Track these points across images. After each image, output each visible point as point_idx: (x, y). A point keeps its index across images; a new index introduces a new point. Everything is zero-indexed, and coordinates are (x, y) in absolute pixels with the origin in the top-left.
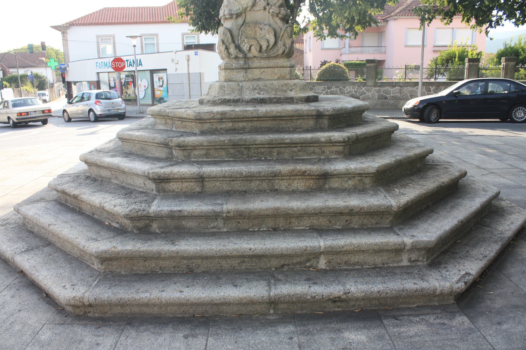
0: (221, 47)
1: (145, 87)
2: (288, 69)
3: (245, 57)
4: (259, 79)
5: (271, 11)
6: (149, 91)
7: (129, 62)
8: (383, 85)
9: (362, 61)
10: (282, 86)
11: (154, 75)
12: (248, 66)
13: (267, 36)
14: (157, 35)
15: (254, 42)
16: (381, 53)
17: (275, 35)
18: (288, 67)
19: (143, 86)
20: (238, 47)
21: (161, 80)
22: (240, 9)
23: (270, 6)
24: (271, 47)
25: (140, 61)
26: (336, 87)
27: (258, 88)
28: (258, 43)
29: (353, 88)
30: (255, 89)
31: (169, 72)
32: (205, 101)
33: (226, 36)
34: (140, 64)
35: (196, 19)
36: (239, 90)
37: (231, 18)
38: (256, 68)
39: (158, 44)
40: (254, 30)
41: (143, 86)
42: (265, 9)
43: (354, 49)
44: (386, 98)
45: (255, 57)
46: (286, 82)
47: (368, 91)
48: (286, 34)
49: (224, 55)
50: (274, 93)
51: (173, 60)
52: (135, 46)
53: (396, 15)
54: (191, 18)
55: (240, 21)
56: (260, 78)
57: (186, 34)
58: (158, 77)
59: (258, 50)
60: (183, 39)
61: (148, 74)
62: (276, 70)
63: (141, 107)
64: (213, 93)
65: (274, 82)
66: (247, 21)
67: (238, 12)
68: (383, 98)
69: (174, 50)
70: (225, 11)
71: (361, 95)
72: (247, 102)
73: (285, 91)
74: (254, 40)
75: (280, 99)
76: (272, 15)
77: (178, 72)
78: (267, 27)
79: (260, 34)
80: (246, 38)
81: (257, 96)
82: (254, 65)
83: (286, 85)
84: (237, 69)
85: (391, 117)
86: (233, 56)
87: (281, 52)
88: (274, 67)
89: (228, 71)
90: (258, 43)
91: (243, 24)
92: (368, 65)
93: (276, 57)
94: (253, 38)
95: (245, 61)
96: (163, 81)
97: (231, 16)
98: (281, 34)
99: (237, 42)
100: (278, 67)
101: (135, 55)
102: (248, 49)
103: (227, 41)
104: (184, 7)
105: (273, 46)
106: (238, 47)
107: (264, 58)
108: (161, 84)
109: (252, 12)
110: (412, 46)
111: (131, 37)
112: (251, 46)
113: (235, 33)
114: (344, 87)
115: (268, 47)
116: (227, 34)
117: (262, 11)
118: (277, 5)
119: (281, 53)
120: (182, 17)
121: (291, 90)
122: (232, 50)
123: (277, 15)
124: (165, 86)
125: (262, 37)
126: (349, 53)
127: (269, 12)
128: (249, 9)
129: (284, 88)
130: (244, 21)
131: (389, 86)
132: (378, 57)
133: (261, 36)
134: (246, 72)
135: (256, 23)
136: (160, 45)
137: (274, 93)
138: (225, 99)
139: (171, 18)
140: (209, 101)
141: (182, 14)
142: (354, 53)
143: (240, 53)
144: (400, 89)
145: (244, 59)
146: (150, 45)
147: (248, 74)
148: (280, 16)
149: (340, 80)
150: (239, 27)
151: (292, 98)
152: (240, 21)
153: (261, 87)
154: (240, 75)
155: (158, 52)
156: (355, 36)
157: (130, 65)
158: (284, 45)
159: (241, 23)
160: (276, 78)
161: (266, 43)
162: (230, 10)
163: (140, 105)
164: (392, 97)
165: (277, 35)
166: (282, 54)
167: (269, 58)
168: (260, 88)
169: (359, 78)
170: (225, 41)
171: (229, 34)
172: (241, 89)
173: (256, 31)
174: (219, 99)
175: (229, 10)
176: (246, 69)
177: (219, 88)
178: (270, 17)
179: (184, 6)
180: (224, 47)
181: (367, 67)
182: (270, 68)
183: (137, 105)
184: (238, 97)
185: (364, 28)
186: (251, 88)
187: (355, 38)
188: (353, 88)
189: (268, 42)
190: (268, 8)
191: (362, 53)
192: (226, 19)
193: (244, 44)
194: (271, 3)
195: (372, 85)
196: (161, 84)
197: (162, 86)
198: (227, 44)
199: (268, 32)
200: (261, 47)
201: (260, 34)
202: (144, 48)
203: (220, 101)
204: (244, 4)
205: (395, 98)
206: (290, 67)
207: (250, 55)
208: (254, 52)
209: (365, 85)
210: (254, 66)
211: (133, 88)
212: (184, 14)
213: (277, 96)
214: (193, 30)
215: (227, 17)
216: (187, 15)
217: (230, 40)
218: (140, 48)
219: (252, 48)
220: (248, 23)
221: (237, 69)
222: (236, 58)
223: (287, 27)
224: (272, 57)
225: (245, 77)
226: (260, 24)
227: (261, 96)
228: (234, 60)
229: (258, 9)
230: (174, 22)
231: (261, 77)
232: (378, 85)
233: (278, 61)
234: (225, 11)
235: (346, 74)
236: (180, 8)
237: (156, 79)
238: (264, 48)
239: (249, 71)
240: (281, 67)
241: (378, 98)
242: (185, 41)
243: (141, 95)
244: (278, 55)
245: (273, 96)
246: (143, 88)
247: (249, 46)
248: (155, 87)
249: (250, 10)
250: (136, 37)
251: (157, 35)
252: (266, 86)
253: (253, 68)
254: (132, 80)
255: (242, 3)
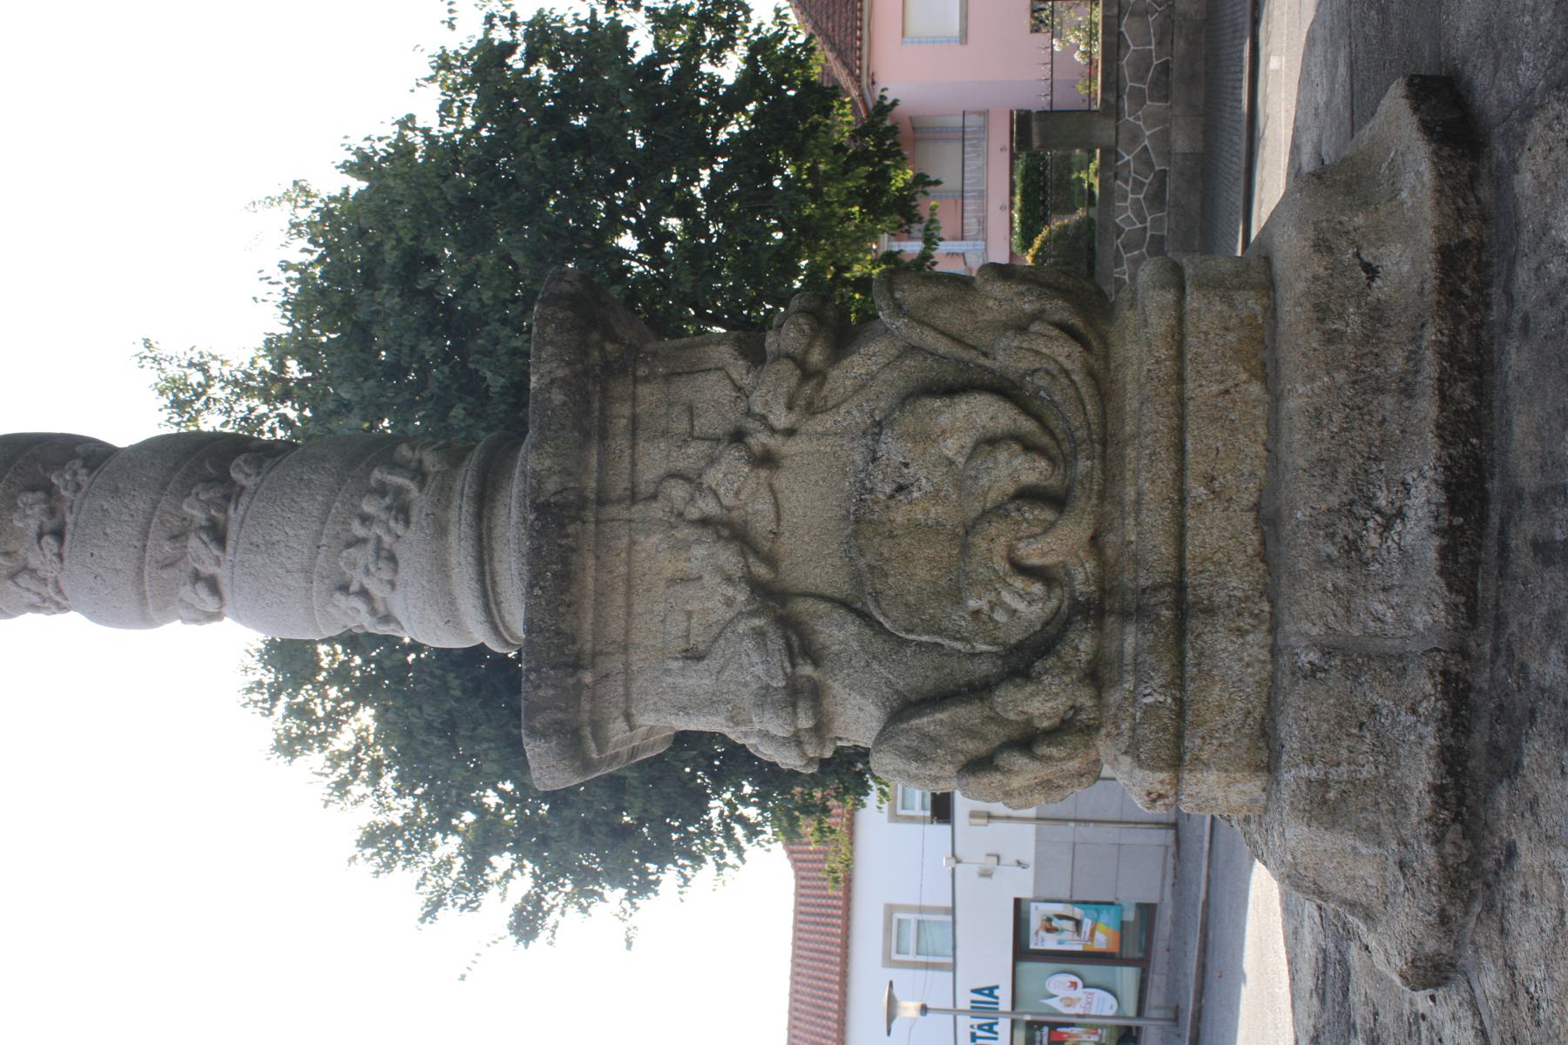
0: (1016, 782)
1: (1074, 985)
2: (1193, 301)
3: (1091, 611)
4: (1267, 519)
5: (781, 419)
6: (1092, 972)
7: (979, 1033)
8: (1112, 83)
9: (1012, 185)
10: (1331, 338)
11: (1032, 946)
12: (1165, 595)
13: (951, 447)
14: (890, 909)
15: (993, 544)
16: (984, 129)
17: (951, 391)
18: (1180, 301)
19: (1071, 993)
20: (1024, 659)
21: (1056, 923)
22: (759, 634)
23: (751, 424)
24: (1027, 425)
25: (974, 991)
26: (1118, 262)
27: (1343, 528)
28: (997, 511)
29: (1125, 198)
30: (1352, 545)
31: (1026, 893)
32: (1431, 946)
33: (935, 741)
34: (991, 995)
35: (842, 781)
36: (1353, 673)
37: (816, 694)
38: (1180, 539)
39: (921, 909)
40: (905, 541)
41: (1071, 993)
42: (767, 460)
43: (971, 224)
44: (1165, 68)
45: (1095, 541)
46: (1293, 311)
47: (1135, 137)
48: (944, 315)
49: (1073, 765)
50: (1389, 402)
51: (985, 874)
52: (924, 1009)
53: (858, 79)
54: (839, 796)
55: (837, 633)
56: (1256, 507)
57: (893, 807)
58: (1043, 934)
59: (1048, 515)
60: (911, 819)
61: (1027, 967)
62: (1201, 390)
63: (1151, 1012)
64: (1367, 871)
65: (1292, 404)
66: (839, 584)
67: (776, 642)
68: (1161, 89)
69: (945, 863)
70: (765, 735)
71: (1152, 166)
72: (1473, 615)
73: (1377, 315)
74: (980, 543)
75: (1449, 353)
76: (811, 410)
77: (1029, 857)
78: (893, 448)
79: (936, 495)
80: (956, 595)
81: (1418, 530)
82: (1160, 546)
83: (1322, 311)
84: (1178, 680)
85: (1247, 32)
86: (1085, 699)
87: (1064, 352)
88: (1181, 402)
89: (1192, 742)
90: (997, 511)
91: (864, 616)
92: (1036, 143)
93: (1103, 384)
94: (965, 548)
95: (1125, 616)
96: (1061, 917)
97: (802, 694)
98: (943, 346)
99: (984, 668)
100: (1180, 379)
101: (955, 1012)
102: (1037, 588)
103: (972, 734)
104: (797, 819)
105: (1027, 411)
106: (1024, 659)
107: (1110, 475)
108: (1069, 925)
109: (786, 544)
110: (964, 17)
111: (891, 1016)
112: (1021, 569)
113: (918, 674)
114: (1119, 231)
115: (1029, 447)
116: (924, 736)
117: (782, 480)
118: (747, 381)
119: (1077, 349)
120: (832, 832)
121: (1371, 271)
122: (1038, 704)
123: (808, 374)
124: (1077, 912)
125: (959, 485)
126: (985, 240)
127: (790, 432)
128: (761, 571)
129: (1353, 322)
130: (844, 604)
131: (1119, 59)
132: (1000, 135)
133: (948, 488)
134: (1211, 611)
135: (860, 521)
136: (925, 902)
137: (1389, 402)
138: (1438, 790)
139: (833, 871)
140: (1444, 919)
141: (821, 830)
142: (983, 222)
143: (1066, 651)
144: (1132, 14)
145: (1110, 621)
146: (926, 939)
147: (1220, 598)
148: (816, 357)
149: (1091, 250)
150: (878, 645)
151: (1450, 257)
152: (837, 633)
153: (1333, 500)
154: (1232, 658)
155: (952, 911)
156: (930, 183)
157: (990, 1030)
158: (1021, 328)
159: (853, 627)
160: (1256, 389)
161: (1002, 456)
162: (764, 696)
163: (1140, 1012)
164: (1159, 43)
165: (950, 375)
166: (1086, 346)
167: (1107, 442)
168: (1347, 510)
169: (1083, 175)
170: (974, 747)
171: (924, 722)
172: (1348, 657)
173: (915, 527)
174: (1438, 841)
175: (760, 706)
176: (1183, 611)
177: (1333, 825)
178: (825, 422)
179: (793, 821)
180: (1019, 760)
181: (1045, 145)
182: (1180, 431)
183: (1138, 1028)
184: (1424, 684)
185: (901, 161)
186: (1341, 578)
187: (937, 183)
188: (1125, 198)
189: (990, 442)
190: (760, 440)
191: (982, 195)
192: (820, 729)
193: (1000, 616)
194: (734, 417)
195: (1112, 123)
196: (1069, 925)
197: (1078, 924)
198: (996, 735)
199: (924, 438)
200: (1028, 495)
201: (936, 495)
202: (931, 959)
203: (1454, 833)
204: (729, 602)
205: (1165, 36)
206: (1181, 289)
207: (1083, 577)
208: (1058, 543)
209: (1110, 154)
210: (1167, 550)
211: (1075, 1030)
212: (820, 822)
213: (1430, 368)
214: (883, 793)
215: (805, 722)
216: (826, 810)
217: (967, 713)
218: (930, 973)
219: (1035, 561)
220: (857, 579)
221: (1178, 680)
222: (1096, 676)
223: (898, 308)
224: (1103, 415)
225: (1246, 622)
226: (864, 490)
227: (1423, 498)
228: (1114, 697)
229: (764, 505)
230: (849, 864)
231: (1248, 499)
232: (1112, 100)
233: (1129, 373)
234: (765, 735)
235: (1066, 227)
236: (800, 836)
237: (1050, 943)
238: (1032, 471)
239: (1200, 585)
240: (1180, 355)
241: (1166, 98)
242: (918, 812)
243: (1103, 1005)
244: (1091, 373)
245: (1427, 407)
246: (1080, 992)
247: (1019, 583)
248: (1078, 948)
249: (771, 561)
250: (892, 1002)
251: (890, 909)
252: (1327, 466)
253: (1180, 557)
254: (1046, 1029)
255: (722, 613)
